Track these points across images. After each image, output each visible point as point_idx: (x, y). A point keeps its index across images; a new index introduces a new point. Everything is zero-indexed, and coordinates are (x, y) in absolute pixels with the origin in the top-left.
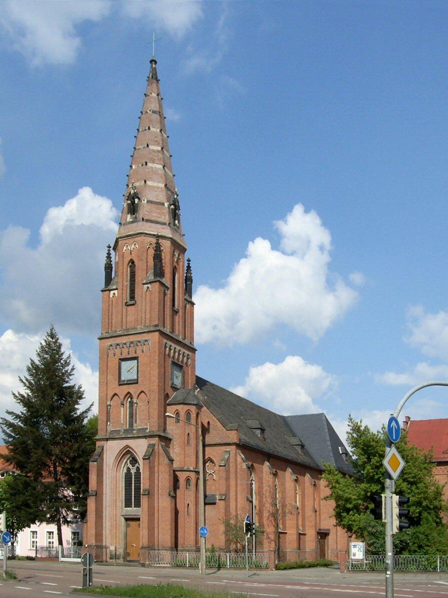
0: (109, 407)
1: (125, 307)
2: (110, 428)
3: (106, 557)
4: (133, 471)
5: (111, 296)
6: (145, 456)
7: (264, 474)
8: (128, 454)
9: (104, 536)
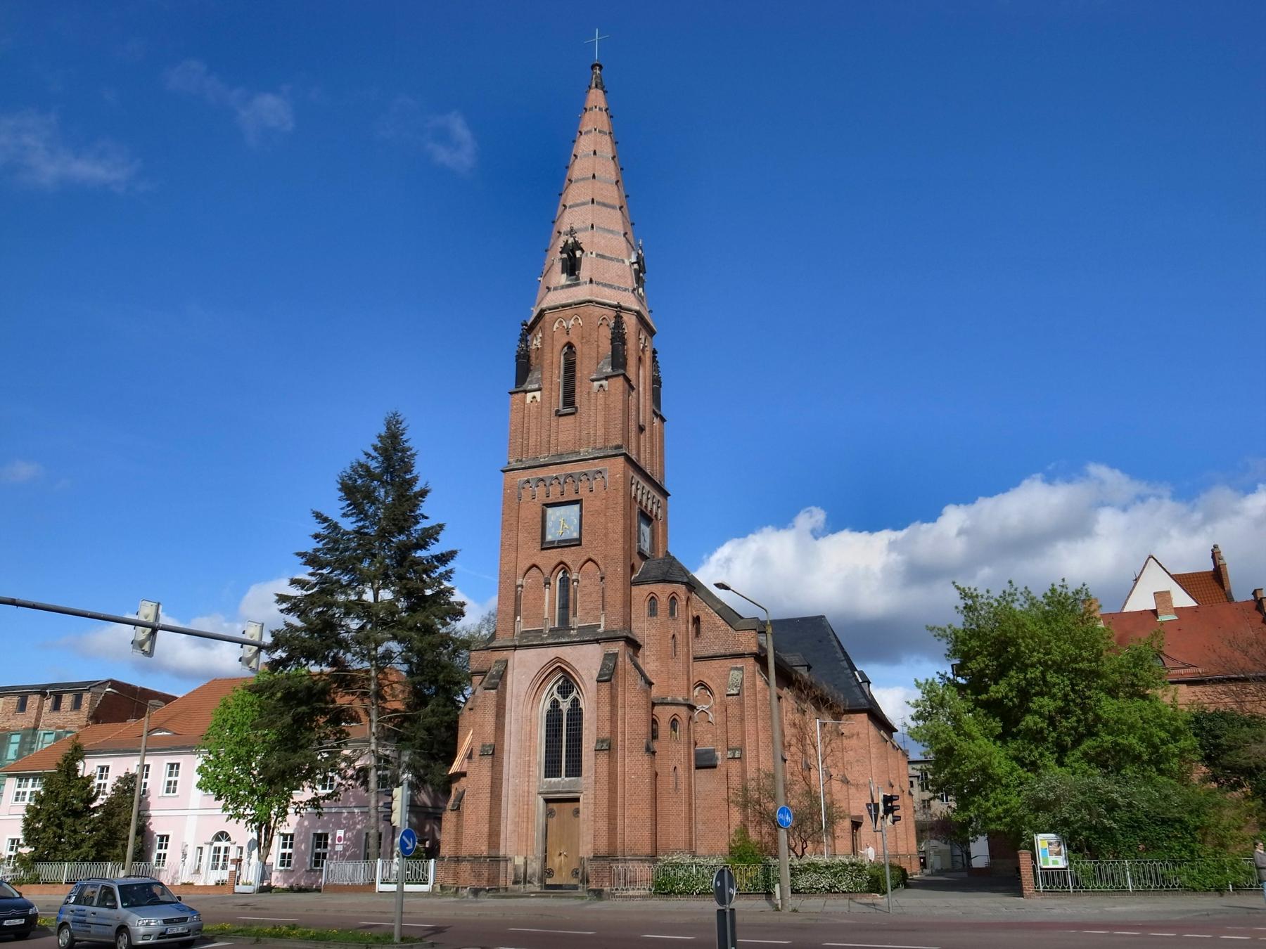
1: (554, 418)
2: (521, 627)
3: (506, 880)
4: (565, 706)
6: (600, 675)
9: (502, 837)
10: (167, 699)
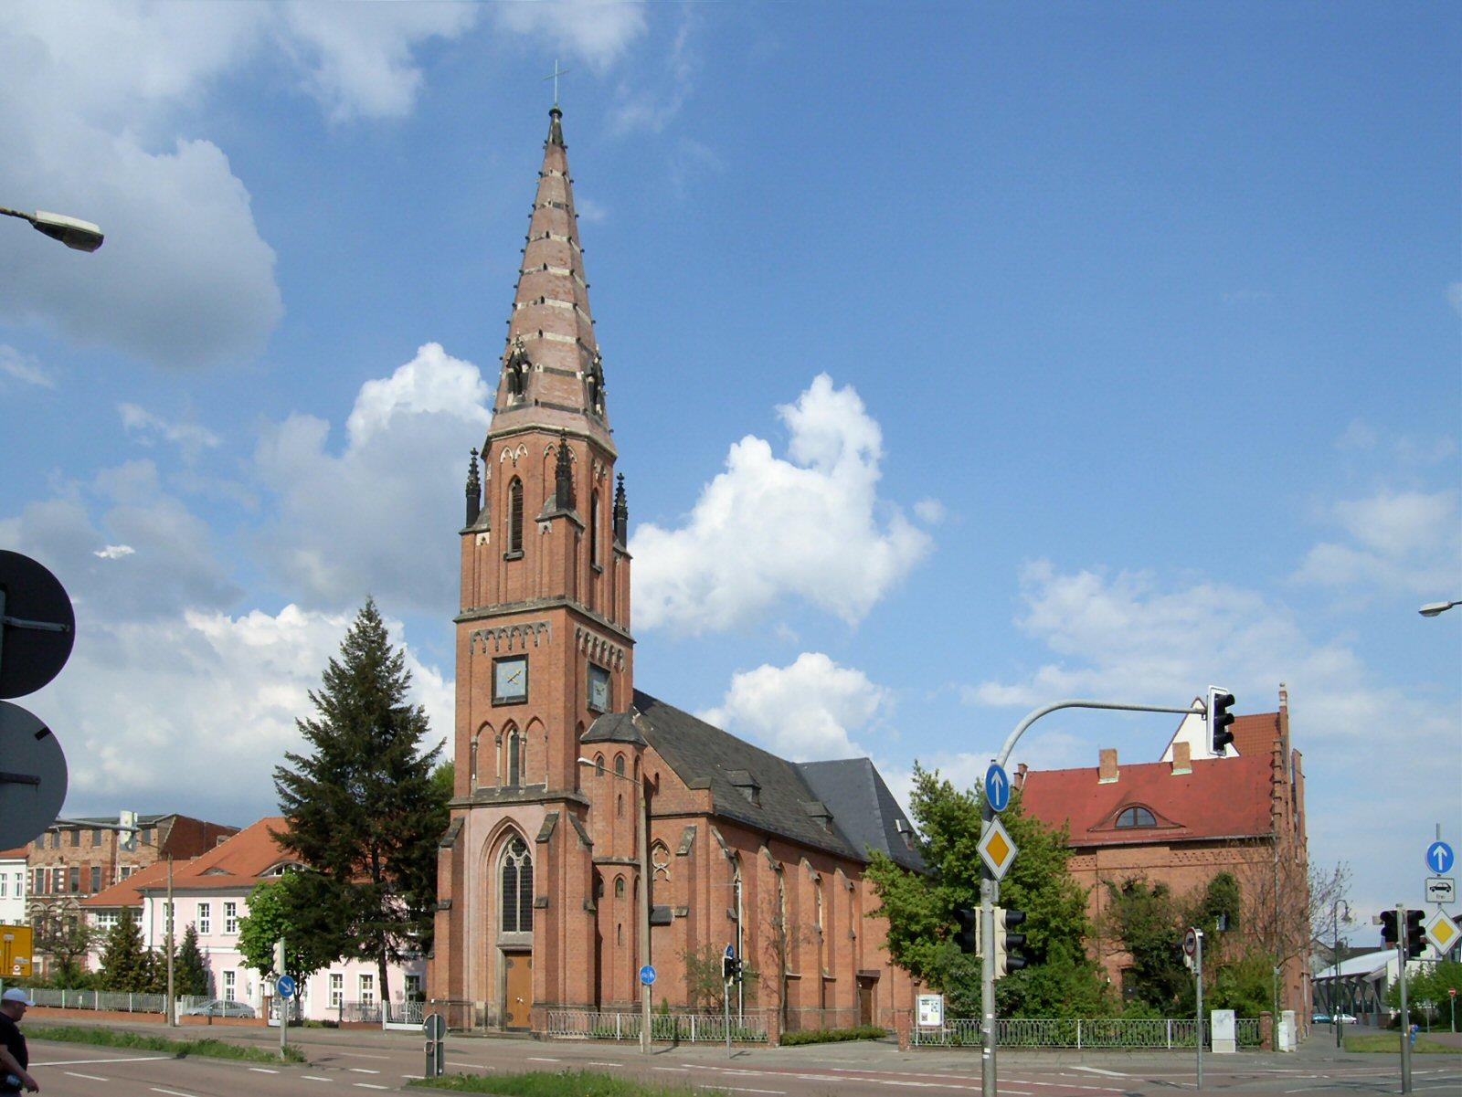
0: (474, 747)
1: (503, 563)
2: (476, 786)
3: (469, 1021)
4: (518, 864)
5: (478, 544)
6: (539, 836)
7: (759, 869)
8: (509, 833)
9: (465, 984)
10: (231, 832)
